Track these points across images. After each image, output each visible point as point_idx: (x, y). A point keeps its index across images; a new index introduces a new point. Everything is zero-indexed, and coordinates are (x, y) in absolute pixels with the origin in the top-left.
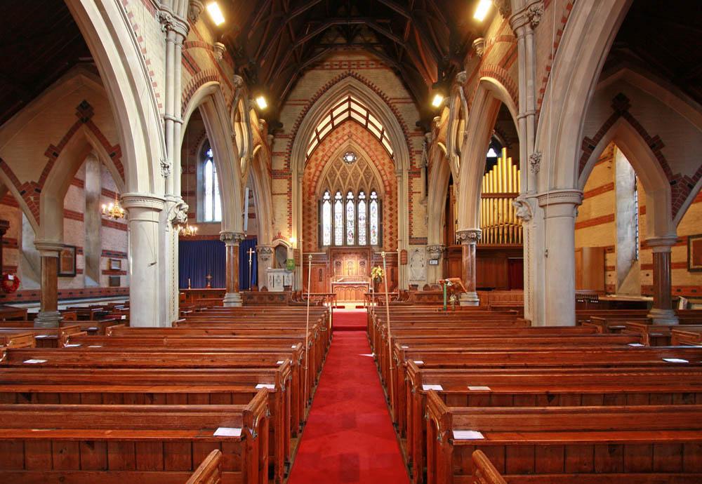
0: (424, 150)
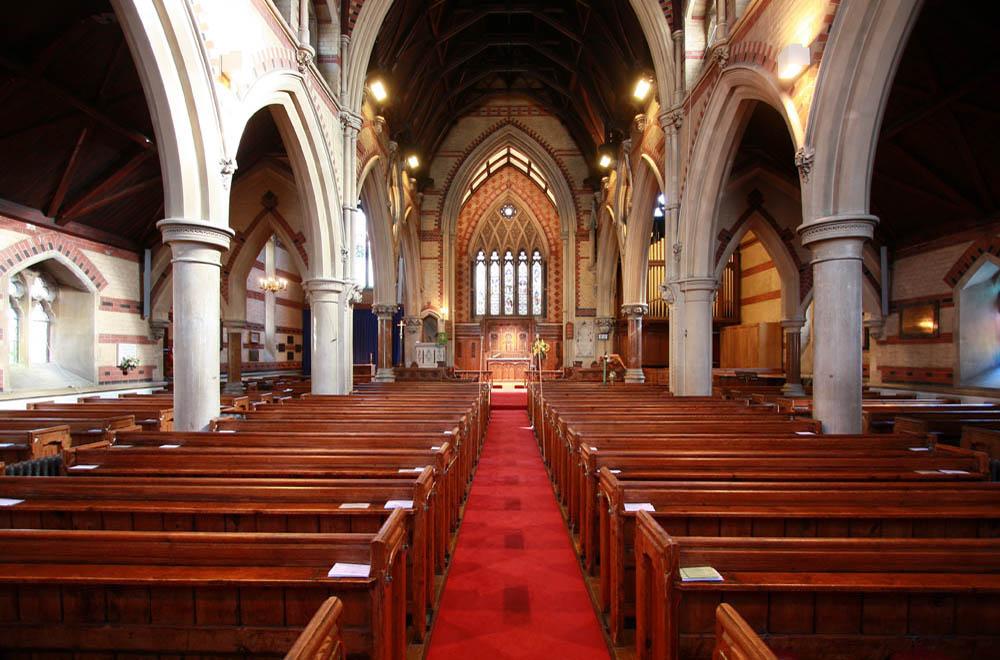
0: (593, 211)
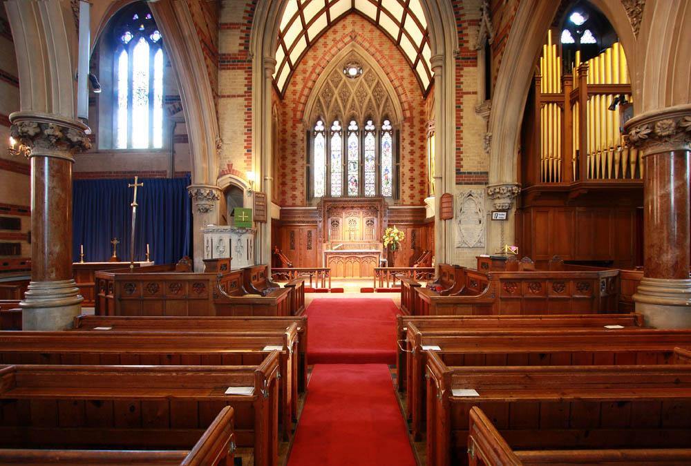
0: (485, 17)
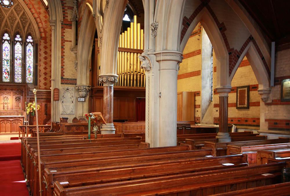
0: (75, 7)
